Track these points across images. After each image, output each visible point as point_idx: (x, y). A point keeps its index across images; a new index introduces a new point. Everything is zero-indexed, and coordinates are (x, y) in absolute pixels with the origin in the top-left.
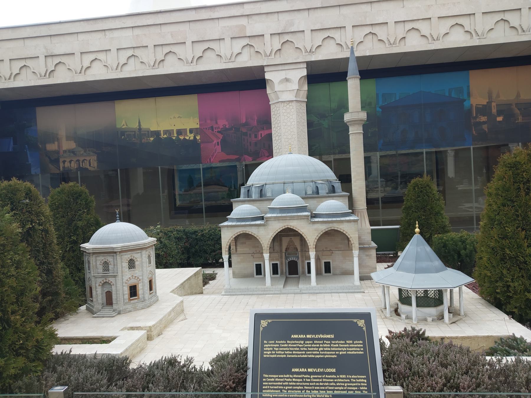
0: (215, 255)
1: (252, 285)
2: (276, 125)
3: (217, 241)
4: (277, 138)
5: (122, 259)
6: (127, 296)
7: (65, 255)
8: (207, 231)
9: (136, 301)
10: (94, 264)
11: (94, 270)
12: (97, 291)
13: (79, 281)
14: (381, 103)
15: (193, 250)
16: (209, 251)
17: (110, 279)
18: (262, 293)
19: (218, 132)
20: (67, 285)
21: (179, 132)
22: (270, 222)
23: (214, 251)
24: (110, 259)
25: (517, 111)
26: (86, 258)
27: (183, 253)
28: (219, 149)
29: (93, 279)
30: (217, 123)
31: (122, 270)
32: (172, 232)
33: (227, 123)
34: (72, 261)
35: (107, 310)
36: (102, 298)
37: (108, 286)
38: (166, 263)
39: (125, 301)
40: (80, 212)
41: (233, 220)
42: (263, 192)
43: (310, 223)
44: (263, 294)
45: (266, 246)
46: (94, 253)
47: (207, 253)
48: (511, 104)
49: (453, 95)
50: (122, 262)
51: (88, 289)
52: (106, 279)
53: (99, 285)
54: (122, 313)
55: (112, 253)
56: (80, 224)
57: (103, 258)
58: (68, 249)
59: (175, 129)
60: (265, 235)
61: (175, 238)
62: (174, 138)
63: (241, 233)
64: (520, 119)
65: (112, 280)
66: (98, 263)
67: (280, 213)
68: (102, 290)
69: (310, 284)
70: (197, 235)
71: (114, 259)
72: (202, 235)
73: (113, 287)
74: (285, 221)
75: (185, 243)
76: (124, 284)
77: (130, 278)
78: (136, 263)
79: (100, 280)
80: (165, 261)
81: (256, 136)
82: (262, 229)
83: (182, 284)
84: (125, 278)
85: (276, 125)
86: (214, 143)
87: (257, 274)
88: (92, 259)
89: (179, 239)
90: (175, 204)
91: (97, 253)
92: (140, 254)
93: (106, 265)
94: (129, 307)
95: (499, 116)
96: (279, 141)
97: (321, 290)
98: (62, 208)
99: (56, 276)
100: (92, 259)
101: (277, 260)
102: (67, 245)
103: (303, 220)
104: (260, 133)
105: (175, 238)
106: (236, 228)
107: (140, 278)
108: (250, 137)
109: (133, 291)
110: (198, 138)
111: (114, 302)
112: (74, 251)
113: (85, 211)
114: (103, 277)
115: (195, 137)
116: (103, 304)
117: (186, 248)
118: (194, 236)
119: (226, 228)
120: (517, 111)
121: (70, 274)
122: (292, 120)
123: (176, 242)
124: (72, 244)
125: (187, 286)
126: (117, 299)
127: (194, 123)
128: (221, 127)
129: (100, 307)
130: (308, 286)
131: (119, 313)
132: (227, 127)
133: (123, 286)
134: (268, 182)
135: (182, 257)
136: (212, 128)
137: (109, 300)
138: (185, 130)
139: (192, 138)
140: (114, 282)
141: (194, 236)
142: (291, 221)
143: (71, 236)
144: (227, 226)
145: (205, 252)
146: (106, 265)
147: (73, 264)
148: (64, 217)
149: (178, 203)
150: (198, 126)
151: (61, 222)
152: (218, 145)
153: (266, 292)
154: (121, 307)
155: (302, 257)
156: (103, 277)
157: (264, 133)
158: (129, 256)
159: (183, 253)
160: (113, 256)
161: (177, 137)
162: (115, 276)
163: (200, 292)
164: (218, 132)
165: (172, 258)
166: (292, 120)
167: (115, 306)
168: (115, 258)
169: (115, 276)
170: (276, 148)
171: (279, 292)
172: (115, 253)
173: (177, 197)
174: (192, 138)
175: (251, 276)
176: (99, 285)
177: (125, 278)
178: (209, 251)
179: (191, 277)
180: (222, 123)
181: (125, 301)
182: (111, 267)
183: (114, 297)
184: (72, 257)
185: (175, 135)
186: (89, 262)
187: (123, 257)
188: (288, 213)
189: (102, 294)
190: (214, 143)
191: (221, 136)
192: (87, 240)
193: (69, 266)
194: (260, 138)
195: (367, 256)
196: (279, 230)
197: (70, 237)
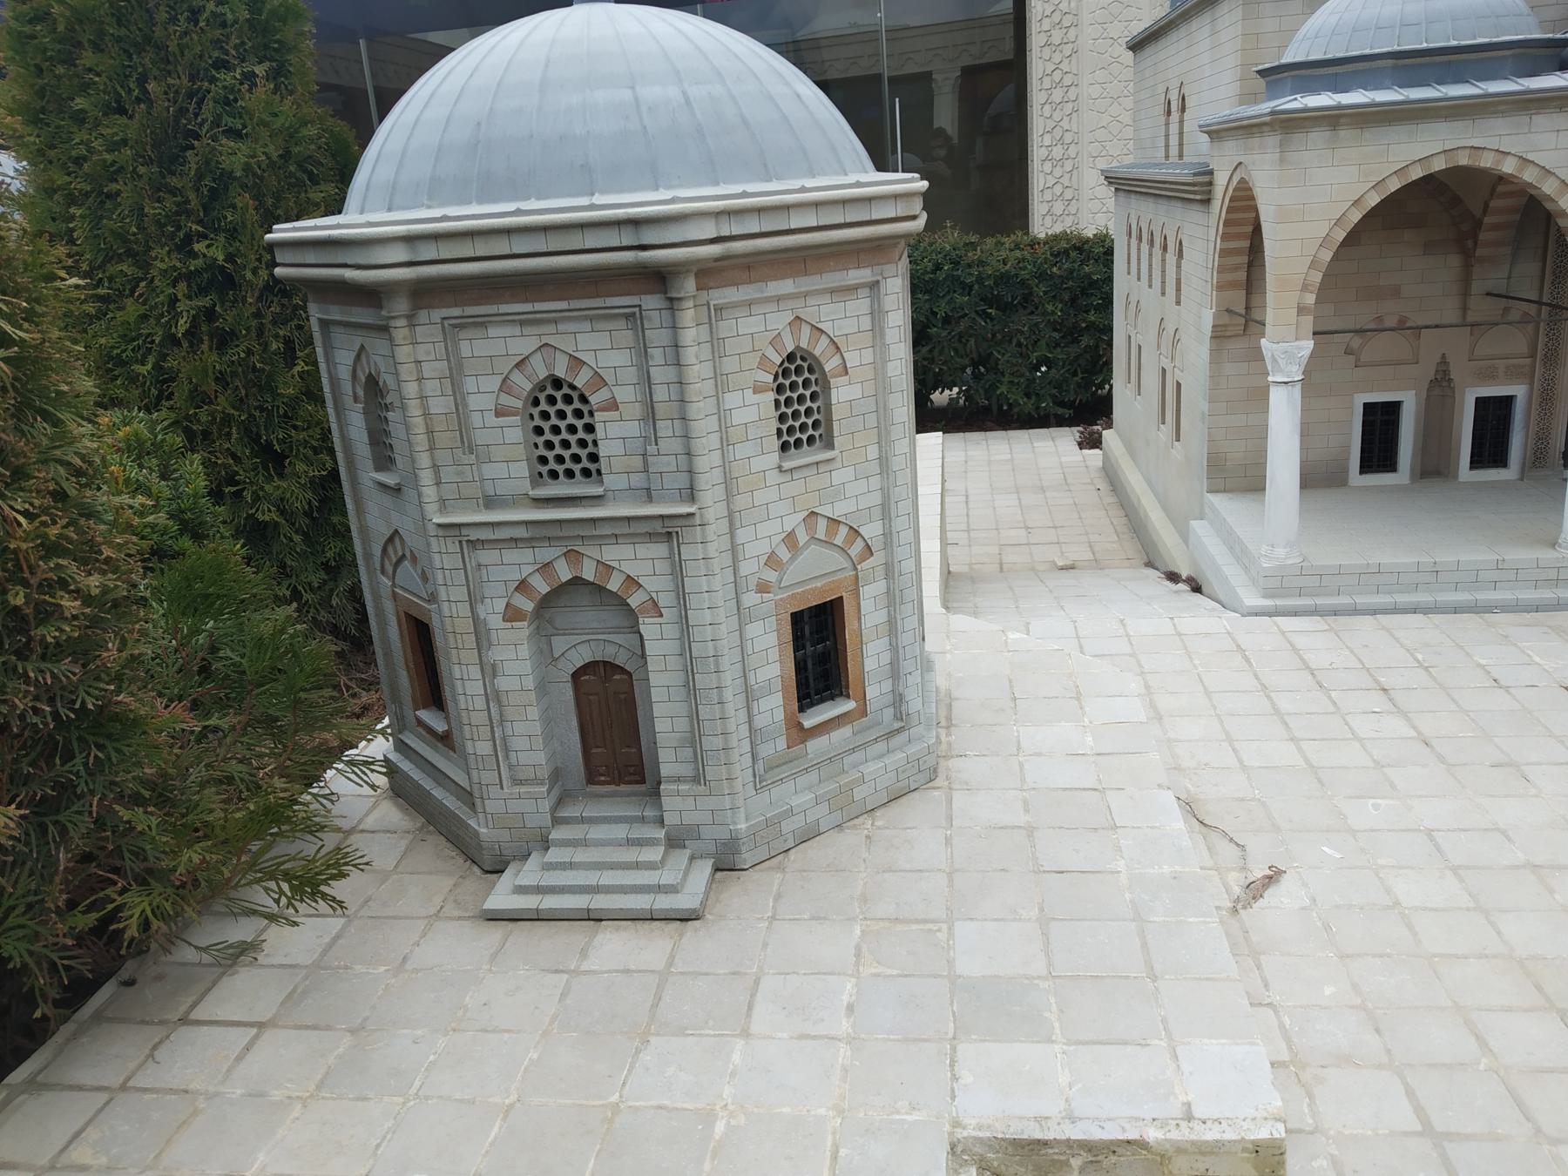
5: (716, 342)
6: (774, 706)
7: (171, 363)
9: (842, 734)
10: (440, 405)
11: (443, 455)
12: (490, 672)
13: (285, 528)
17: (611, 554)
20: (194, 601)
24: (598, 351)
26: (344, 359)
29: (444, 558)
31: (725, 465)
34: (223, 404)
35: (604, 848)
36: (548, 720)
37: (590, 616)
39: (766, 750)
40: (226, 78)
46: (425, 293)
50: (721, 383)
51: (389, 635)
52: (572, 556)
53: (512, 614)
54: (747, 857)
55: (636, 277)
56: (234, 156)
57: (523, 344)
58: (183, 325)
65: (638, 563)
66: (482, 394)
68: (546, 658)
71: (643, 352)
73: (648, 627)
76: (751, 599)
77: (790, 539)
78: (842, 394)
79: (520, 563)
84: (759, 540)
87: (1367, 466)
88: (416, 358)
91: (475, 285)
92: (861, 304)
93: (562, 422)
94: (798, 797)
98: (97, 48)
99: (52, 550)
100: (416, 358)
101: (1513, 375)
102: (174, 300)
107: (871, 531)
109: (820, 651)
111: (670, 762)
112: (223, 341)
113: (260, 70)
114: (539, 534)
116: (556, 775)
121: (216, 495)
124: (203, 291)
126: (694, 739)
129: (534, 806)
131: (726, 864)
133: (743, 616)
137: (612, 740)
140: (656, 582)
143: (189, 239)
146: (562, 422)
147: (227, 420)
148: (122, 111)
151: (113, 147)
154: (745, 813)
156: (539, 534)
158: (779, 320)
160: (634, 319)
162: (667, 531)
167: (678, 804)
168: (657, 337)
169: (667, 531)
172: (659, 279)
176: (512, 614)
177: (759, 540)
181: (766, 750)
182: (615, 436)
183: (665, 717)
184: (221, 379)
186: (374, 390)
187: (725, 327)
189: (542, 688)
192: (327, 176)
193: (206, 434)
197: (185, 247)
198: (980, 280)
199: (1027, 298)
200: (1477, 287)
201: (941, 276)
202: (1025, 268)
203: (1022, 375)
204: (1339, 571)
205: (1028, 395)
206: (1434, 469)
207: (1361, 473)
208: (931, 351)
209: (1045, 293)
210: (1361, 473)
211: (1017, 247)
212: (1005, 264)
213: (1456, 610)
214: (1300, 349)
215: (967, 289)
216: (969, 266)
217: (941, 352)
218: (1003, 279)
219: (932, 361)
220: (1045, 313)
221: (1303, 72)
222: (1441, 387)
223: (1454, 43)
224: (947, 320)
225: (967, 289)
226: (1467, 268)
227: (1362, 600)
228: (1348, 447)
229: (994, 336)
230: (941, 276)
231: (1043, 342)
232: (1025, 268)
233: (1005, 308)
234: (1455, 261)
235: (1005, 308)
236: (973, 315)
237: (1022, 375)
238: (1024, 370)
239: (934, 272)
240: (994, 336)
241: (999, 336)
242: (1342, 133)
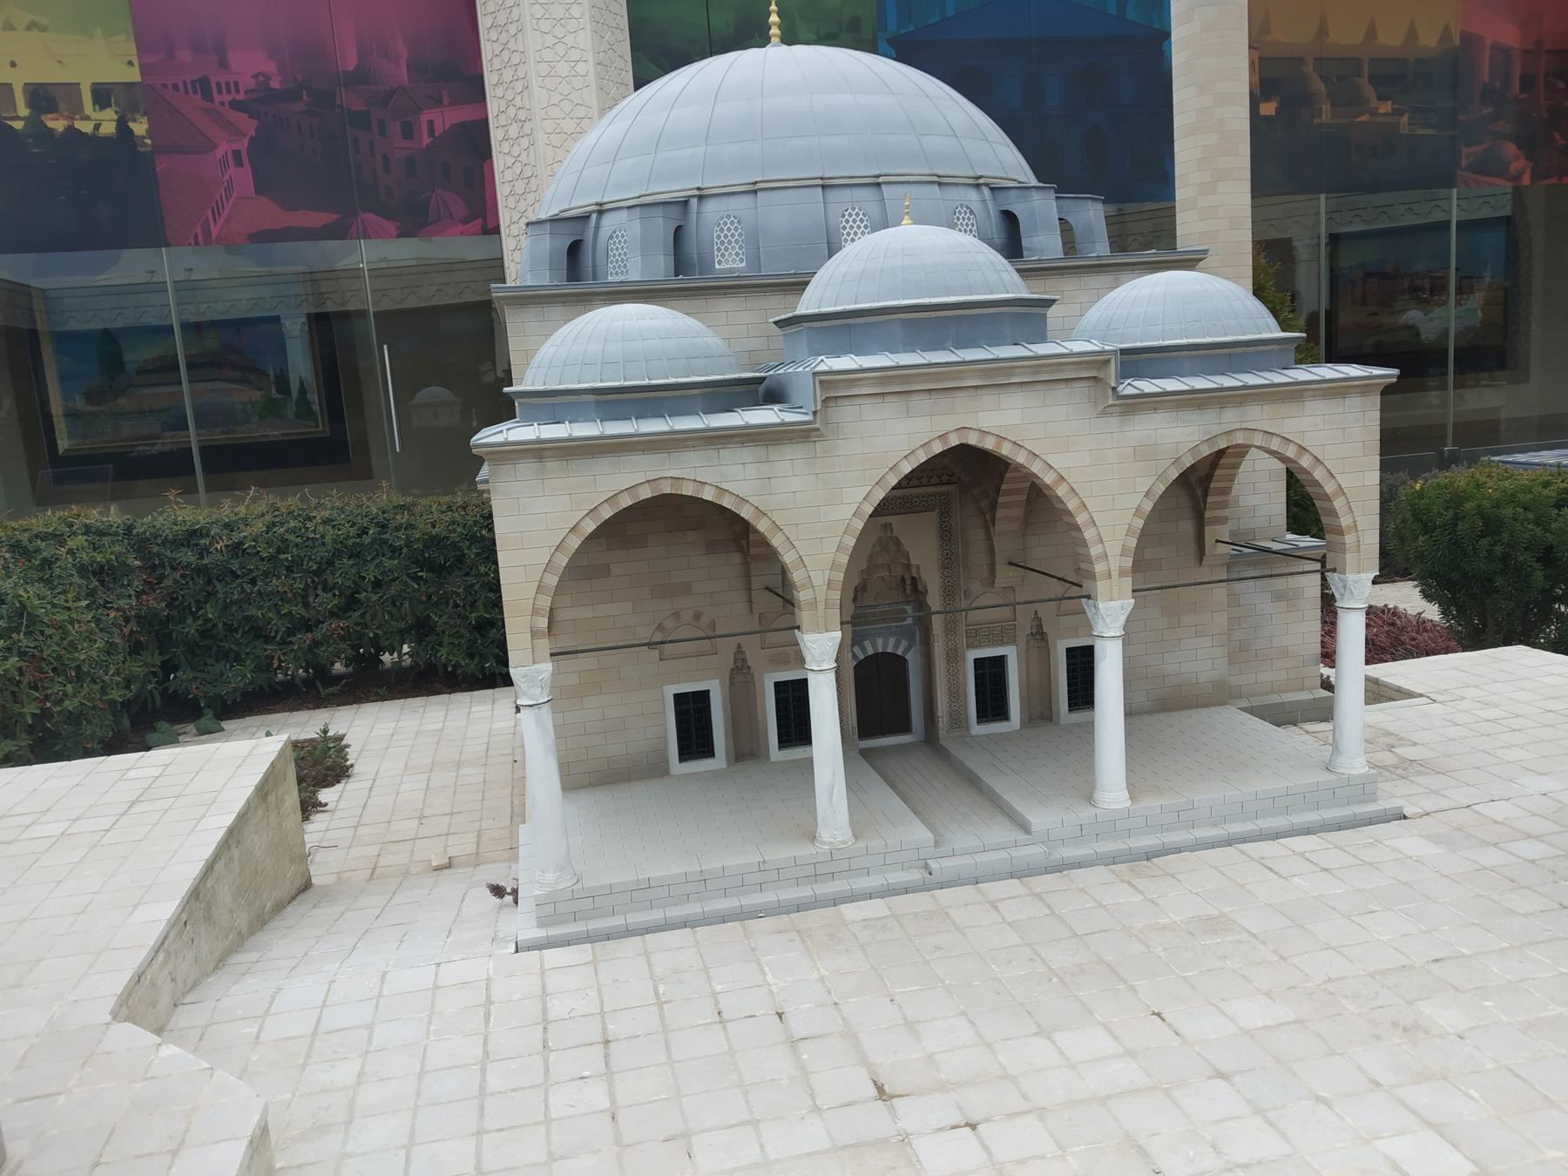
0: (316, 644)
1: (693, 837)
2: (508, 75)
3: (316, 573)
4: (513, 131)
8: (259, 526)
14: (892, 26)
15: (191, 628)
16: (279, 626)
18: (804, 892)
19: (235, 105)
21: (43, 97)
22: (846, 413)
23: (307, 626)
25: (1319, 86)
27: (136, 649)
28: (244, 177)
30: (223, 63)
32: (59, 539)
33: (270, 67)
38: (45, 714)
41: (555, 403)
42: (691, 247)
43: (1104, 413)
44: (815, 903)
45: (819, 579)
47: (268, 639)
48: (1302, 60)
49: (1131, 15)
59: (18, 81)
60: (816, 506)
61: (83, 570)
62: (18, 125)
63: (645, 493)
64: (1327, 114)
67: (909, 347)
69: (1089, 798)
70: (203, 552)
72: (236, 549)
74: (944, 401)
75: (139, 594)
80: (31, 709)
81: (408, 132)
82: (790, 467)
83: (196, 893)
85: (508, 75)
86: (219, 153)
87: (686, 753)
89: (104, 575)
90: (52, 444)
95: (1268, 100)
96: (525, 142)
97: (1163, 828)
103: (1062, 390)
104: (424, 118)
105: (83, 570)
106: (602, 465)
108: (383, 133)
110: (140, 127)
115: (122, 124)
117: (145, 620)
118: (188, 557)
119: (526, 468)
120: (1319, 86)
122: (574, 55)
123: (91, 594)
125: (225, 894)
127: (115, 61)
128: (247, 82)
130: (1085, 814)
132: (275, 84)
134: (711, 182)
135: (137, 669)
136: (204, 87)
138: (73, 88)
139: (109, 129)
141: (188, 557)
142: (988, 398)
144: (538, 451)
145: (259, 633)
149: (63, 444)
150: (134, 75)
152: (239, 163)
153: (839, 886)
155: (950, 630)
157: (446, 118)
159: (136, 649)
161: (34, 121)
163: (298, 882)
164: (235, 105)
165: (79, 678)
166: (574, 55)
170: (508, 175)
171: (915, 876)
173: (60, 426)
174: (109, 129)
175: (654, 769)
178: (279, 626)
179: (243, 817)
180: (250, 65)
185: (23, 110)
188: (961, 344)
190: (219, 153)
191: (249, 126)
194: (426, 141)
195: (1279, 597)
196: (907, 468)
198: (409, 544)
199: (461, 559)
200: (757, 583)
201: (367, 540)
202: (454, 531)
203: (462, 637)
204: (611, 891)
205: (471, 656)
206: (746, 751)
207: (681, 761)
208: (363, 616)
209: (477, 555)
210: (681, 761)
211: (449, 508)
212: (434, 526)
213: (724, 918)
214: (540, 672)
215: (395, 551)
216: (397, 529)
217: (374, 617)
218: (433, 541)
219: (366, 626)
220: (478, 575)
221: (531, 400)
222: (740, 676)
223: (646, 382)
224: (377, 584)
225: (395, 551)
226: (746, 564)
227: (636, 918)
228: (665, 738)
229: (429, 598)
230: (367, 540)
231: (479, 603)
232: (454, 531)
233: (438, 570)
234: (736, 558)
235: (438, 570)
236: (405, 578)
237: (462, 637)
238: (463, 631)
239: (359, 536)
240: (429, 598)
241: (434, 599)
242: (548, 465)
